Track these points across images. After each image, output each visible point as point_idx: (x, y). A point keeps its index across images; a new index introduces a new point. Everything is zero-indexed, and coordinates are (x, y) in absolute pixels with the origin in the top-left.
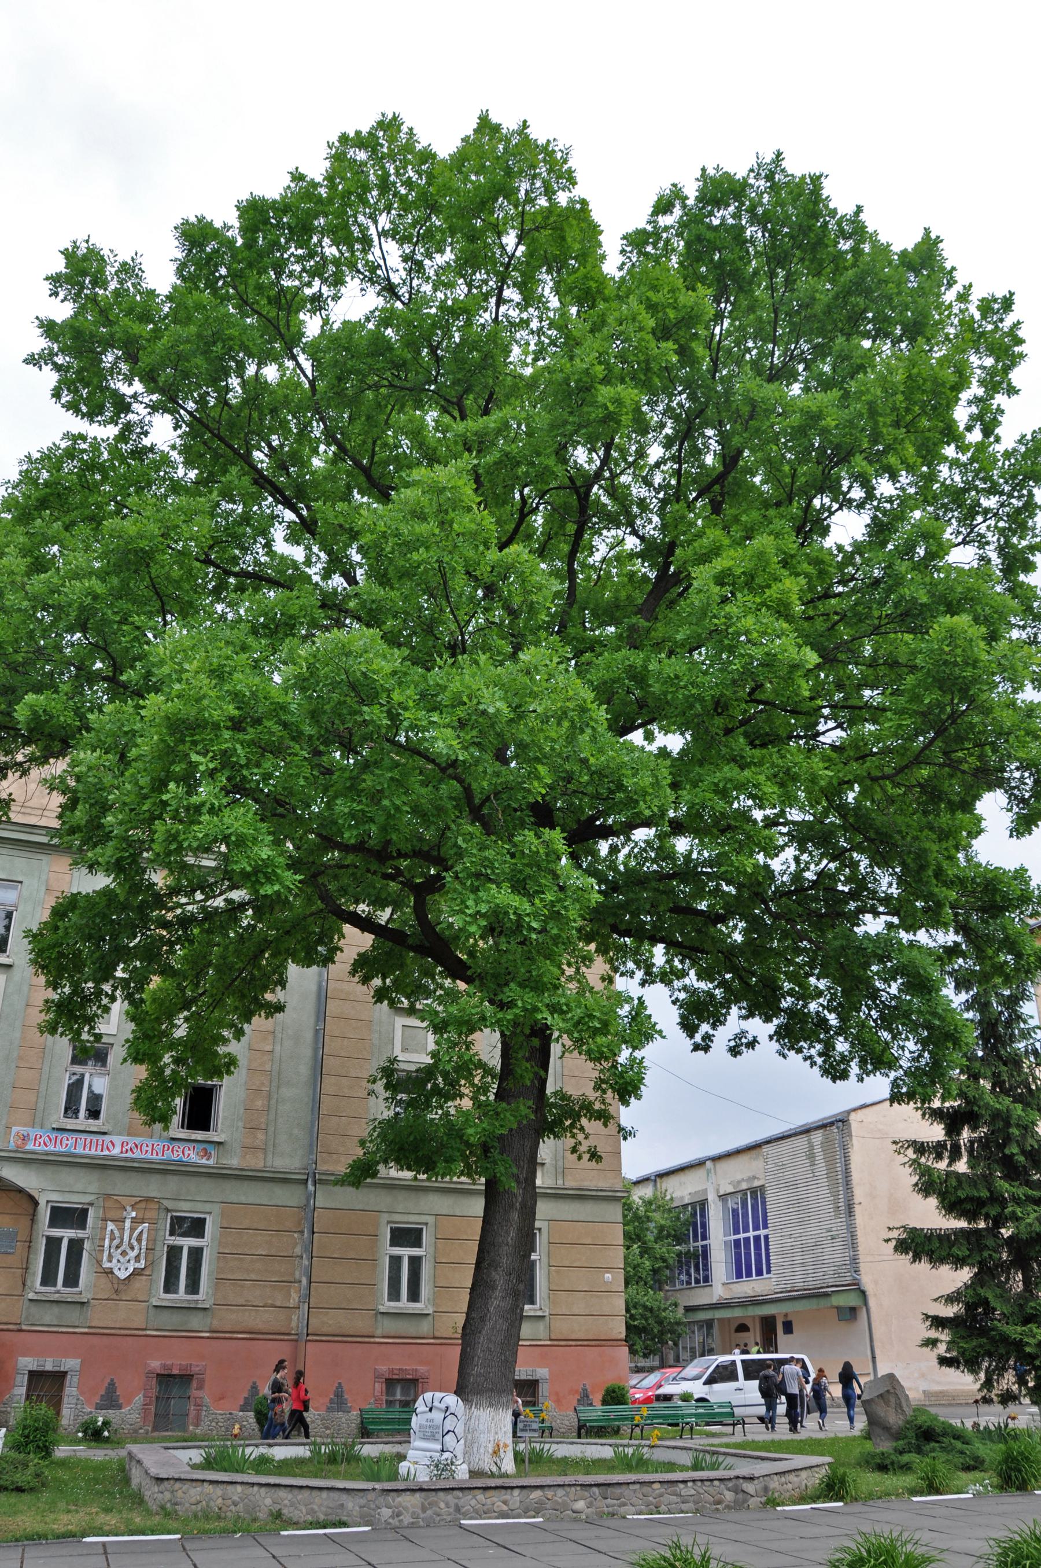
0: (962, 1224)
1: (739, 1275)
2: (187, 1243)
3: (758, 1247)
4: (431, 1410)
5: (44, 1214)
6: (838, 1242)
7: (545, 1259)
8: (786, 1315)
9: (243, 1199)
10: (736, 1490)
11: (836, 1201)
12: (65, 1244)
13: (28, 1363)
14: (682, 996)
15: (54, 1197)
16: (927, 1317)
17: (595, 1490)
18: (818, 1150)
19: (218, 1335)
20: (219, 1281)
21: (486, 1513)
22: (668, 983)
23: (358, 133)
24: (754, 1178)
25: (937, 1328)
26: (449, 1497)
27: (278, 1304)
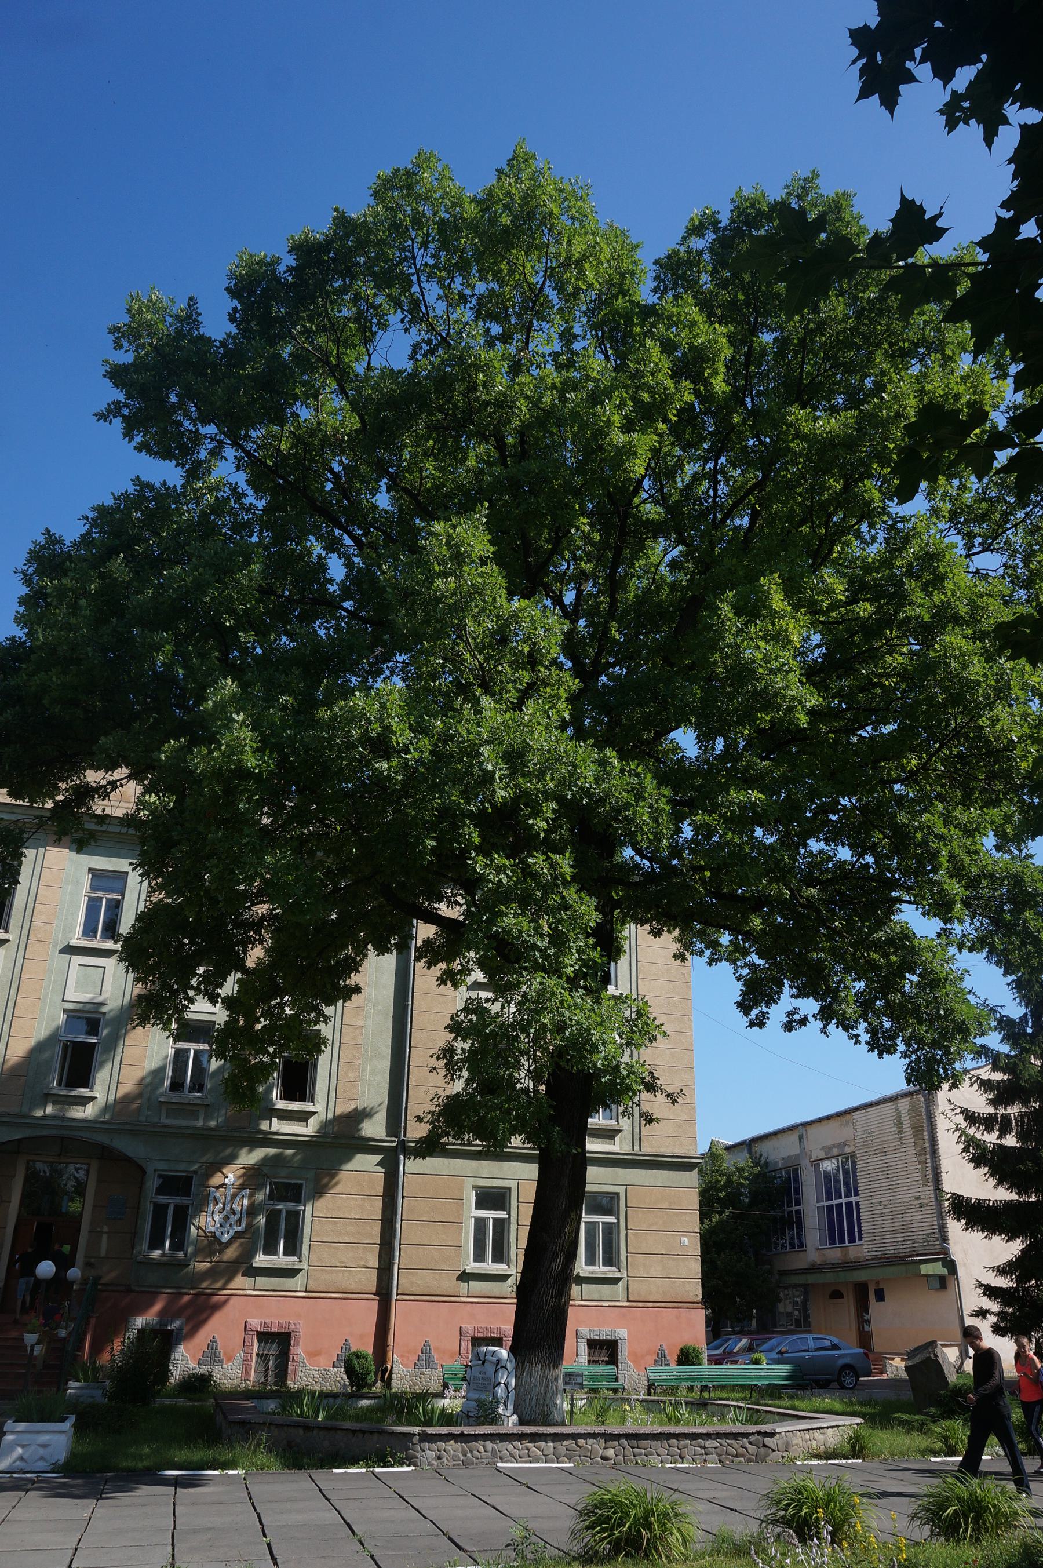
0: (1013, 1196)
1: (833, 1241)
4: (483, 1363)
5: (153, 1183)
6: (926, 1210)
11: (924, 1170)
12: (171, 1208)
14: (745, 972)
15: (162, 1166)
16: (981, 1285)
18: (905, 1117)
22: (733, 962)
23: (23, 601)
24: (845, 1144)
25: (989, 1297)
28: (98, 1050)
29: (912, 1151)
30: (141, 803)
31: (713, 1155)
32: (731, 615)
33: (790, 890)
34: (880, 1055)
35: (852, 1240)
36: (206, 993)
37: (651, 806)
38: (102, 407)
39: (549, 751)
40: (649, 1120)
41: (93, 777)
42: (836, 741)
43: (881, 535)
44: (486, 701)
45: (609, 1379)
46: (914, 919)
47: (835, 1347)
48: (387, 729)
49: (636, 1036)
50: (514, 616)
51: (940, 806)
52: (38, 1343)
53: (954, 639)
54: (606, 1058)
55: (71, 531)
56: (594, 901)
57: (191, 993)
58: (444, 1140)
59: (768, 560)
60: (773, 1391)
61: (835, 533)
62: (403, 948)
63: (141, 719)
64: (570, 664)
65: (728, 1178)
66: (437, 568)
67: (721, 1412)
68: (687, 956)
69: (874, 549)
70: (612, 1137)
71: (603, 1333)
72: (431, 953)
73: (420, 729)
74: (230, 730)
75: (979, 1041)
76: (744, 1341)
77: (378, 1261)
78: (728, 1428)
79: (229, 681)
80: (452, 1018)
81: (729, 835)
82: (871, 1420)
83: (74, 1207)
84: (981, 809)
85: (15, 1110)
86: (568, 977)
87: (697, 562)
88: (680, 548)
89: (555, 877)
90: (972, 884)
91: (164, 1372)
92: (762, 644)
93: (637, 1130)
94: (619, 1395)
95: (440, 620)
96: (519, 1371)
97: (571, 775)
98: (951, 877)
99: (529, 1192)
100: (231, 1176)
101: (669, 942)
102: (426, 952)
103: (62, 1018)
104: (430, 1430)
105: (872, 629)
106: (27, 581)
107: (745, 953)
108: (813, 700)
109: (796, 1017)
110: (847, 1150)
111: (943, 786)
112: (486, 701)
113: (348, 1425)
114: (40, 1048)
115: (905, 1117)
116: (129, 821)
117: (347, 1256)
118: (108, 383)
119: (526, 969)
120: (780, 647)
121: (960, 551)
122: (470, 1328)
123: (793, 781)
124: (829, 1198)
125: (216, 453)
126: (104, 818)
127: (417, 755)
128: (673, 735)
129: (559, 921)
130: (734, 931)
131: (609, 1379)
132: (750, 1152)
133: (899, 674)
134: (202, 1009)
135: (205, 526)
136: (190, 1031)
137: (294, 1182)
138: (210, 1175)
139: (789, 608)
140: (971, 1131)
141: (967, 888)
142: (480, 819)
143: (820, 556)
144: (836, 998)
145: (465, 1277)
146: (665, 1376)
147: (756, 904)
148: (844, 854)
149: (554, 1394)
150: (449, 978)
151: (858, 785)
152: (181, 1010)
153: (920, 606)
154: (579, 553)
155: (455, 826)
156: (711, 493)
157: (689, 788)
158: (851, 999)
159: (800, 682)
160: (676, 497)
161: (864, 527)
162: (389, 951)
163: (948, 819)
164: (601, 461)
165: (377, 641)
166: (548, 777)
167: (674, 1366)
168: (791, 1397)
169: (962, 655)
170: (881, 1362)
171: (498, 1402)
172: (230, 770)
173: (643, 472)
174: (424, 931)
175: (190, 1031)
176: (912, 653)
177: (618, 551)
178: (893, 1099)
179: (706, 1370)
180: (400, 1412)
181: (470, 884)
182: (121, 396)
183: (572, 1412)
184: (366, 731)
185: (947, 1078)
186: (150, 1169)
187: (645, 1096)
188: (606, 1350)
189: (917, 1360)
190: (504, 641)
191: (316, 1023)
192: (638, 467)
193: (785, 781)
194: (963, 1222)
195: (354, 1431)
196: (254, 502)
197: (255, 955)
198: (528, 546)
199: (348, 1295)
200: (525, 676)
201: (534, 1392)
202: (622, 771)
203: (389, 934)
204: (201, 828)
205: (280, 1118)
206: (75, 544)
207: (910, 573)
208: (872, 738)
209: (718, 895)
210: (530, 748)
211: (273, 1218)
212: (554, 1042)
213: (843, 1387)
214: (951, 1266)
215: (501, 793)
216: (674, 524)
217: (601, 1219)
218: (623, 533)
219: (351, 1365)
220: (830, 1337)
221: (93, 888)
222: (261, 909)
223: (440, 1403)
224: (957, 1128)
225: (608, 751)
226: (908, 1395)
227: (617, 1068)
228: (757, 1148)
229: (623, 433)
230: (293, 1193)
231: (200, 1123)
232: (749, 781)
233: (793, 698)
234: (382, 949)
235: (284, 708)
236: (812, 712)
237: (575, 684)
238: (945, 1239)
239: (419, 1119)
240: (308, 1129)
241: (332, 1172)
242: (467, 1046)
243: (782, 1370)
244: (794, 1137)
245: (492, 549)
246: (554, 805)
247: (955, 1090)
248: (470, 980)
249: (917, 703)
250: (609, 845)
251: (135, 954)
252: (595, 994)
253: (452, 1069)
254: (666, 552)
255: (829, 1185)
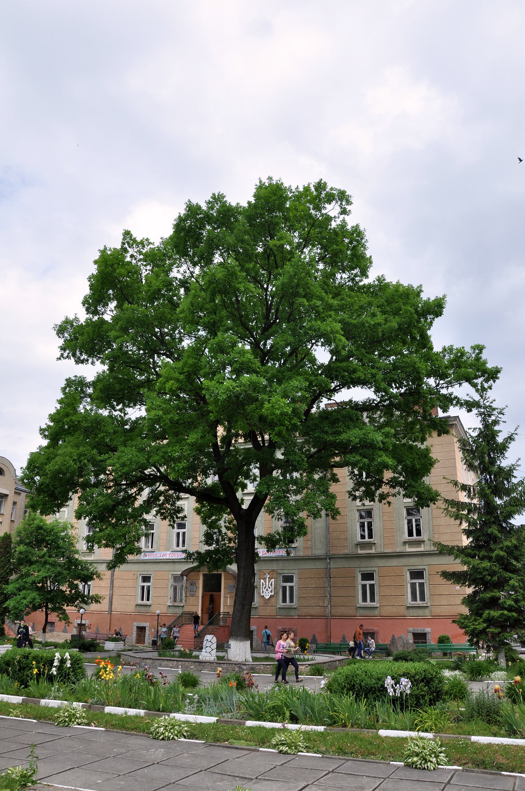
2: (288, 585)
7: (428, 582)
9: (305, 567)
10: (240, 668)
12: (417, 584)
13: (136, 624)
17: (197, 663)
19: (300, 617)
20: (299, 598)
21: (167, 667)
26: (158, 661)
27: (321, 605)
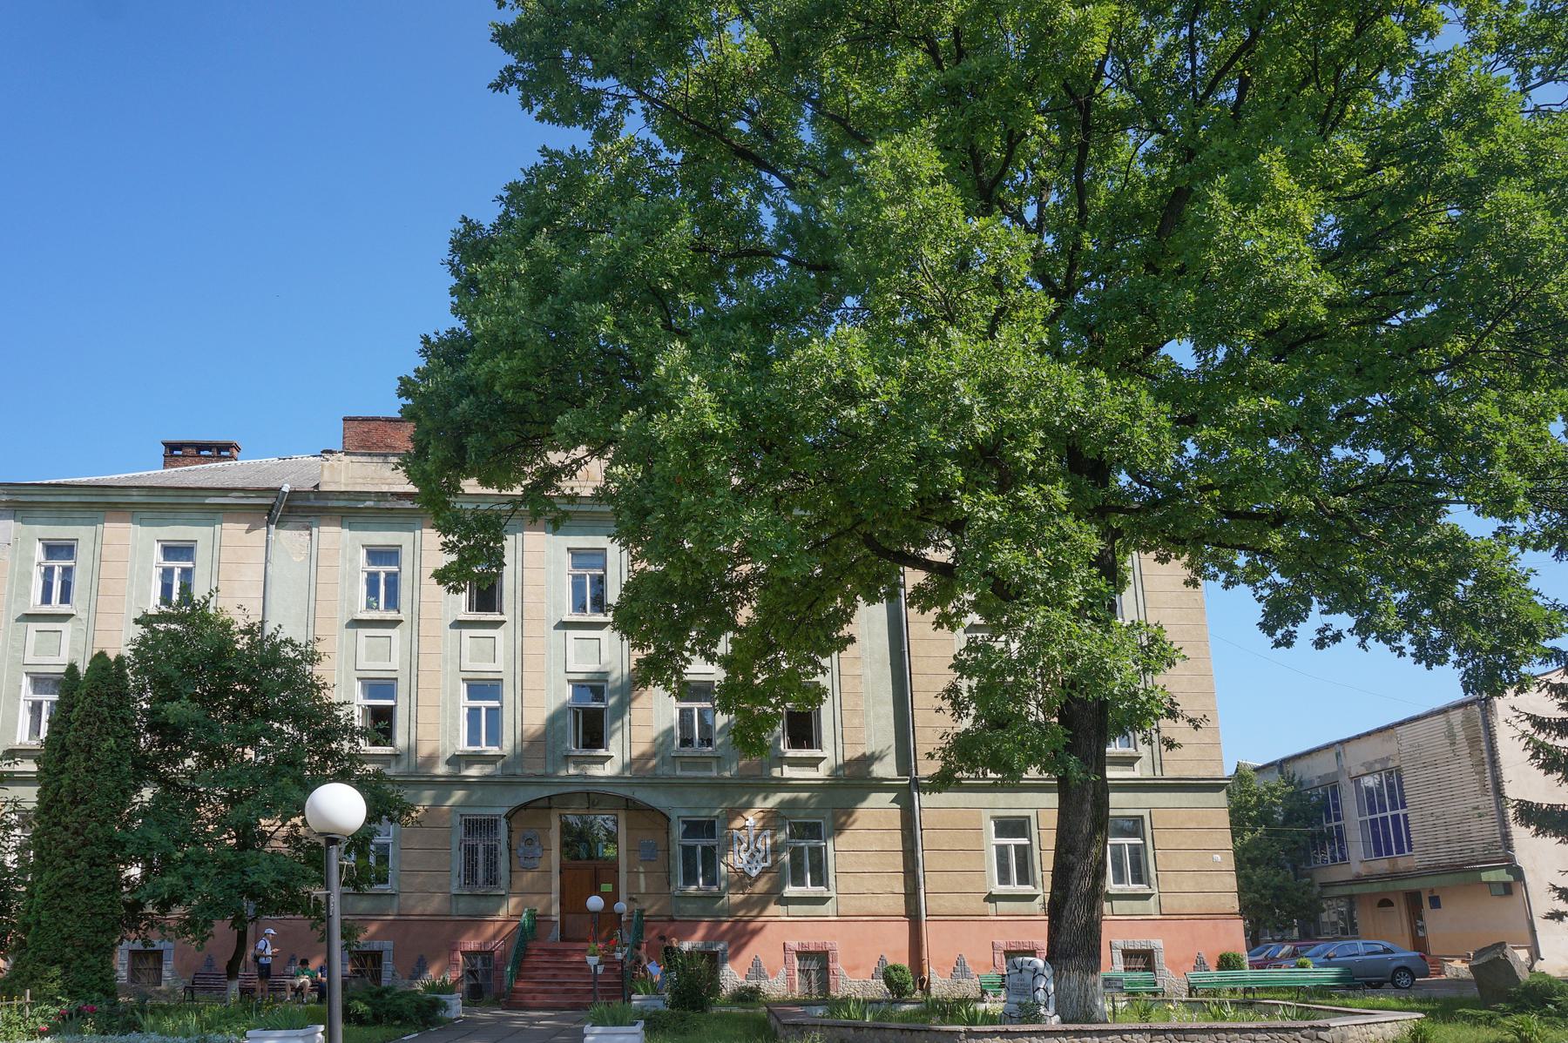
1: (1378, 853)
3: (1385, 826)
5: (678, 830)
8: (1432, 891)
14: (1266, 592)
15: (684, 813)
16: (1555, 888)
18: (1458, 729)
22: (1252, 583)
24: (1388, 759)
28: (607, 716)
29: (1468, 762)
30: (609, 477)
31: (1241, 776)
32: (1224, 204)
33: (1315, 501)
34: (1429, 667)
35: (1400, 850)
36: (703, 653)
37: (1149, 425)
38: (495, 77)
39: (1030, 377)
40: (1171, 745)
41: (555, 458)
42: (1360, 336)
43: (1406, 84)
44: (953, 333)
45: (1148, 983)
46: (1467, 521)
47: (1387, 951)
48: (851, 373)
49: (1153, 662)
50: (976, 237)
51: (1493, 394)
52: (600, 963)
53: (1510, 194)
54: (1122, 685)
55: (488, 215)
56: (1095, 529)
57: (687, 654)
58: (958, 775)
59: (1267, 130)
60: (1322, 992)
61: (1347, 90)
62: (892, 596)
63: (601, 391)
64: (1040, 286)
65: (1259, 797)
66: (883, 195)
67: (1270, 1010)
68: (1200, 580)
69: (1395, 105)
70: (1132, 764)
71: (1138, 944)
72: (922, 598)
73: (886, 371)
74: (685, 392)
75: (1549, 644)
76: (1287, 948)
77: (915, 884)
78: (1278, 1023)
79: (678, 344)
80: (955, 657)
81: (1238, 451)
82: (1432, 1015)
83: (610, 852)
84: (1547, 390)
85: (542, 771)
86: (1073, 609)
87: (1178, 149)
88: (1156, 137)
89: (1051, 508)
90: (1539, 474)
91: (715, 987)
92: (1265, 232)
93: (1157, 756)
94: (1160, 997)
95: (899, 250)
96: (1057, 978)
97: (1057, 400)
98: (1511, 469)
99: (1051, 819)
100: (751, 819)
101: (1177, 569)
102: (919, 597)
103: (568, 691)
104: (975, 1028)
105: (1396, 199)
106: (456, 272)
107: (1265, 573)
108: (1331, 289)
109: (1328, 633)
110: (1391, 764)
111: (1496, 370)
112: (953, 333)
113: (894, 1025)
114: (553, 720)
115: (1458, 729)
116: (601, 496)
117: (870, 883)
118: (496, 49)
119: (1027, 604)
120: (1283, 233)
121: (1513, 87)
122: (1002, 943)
123: (1312, 382)
124: (1373, 811)
125: (623, 105)
126: (573, 498)
127: (886, 398)
128: (1163, 351)
129: (1059, 552)
130: (1252, 550)
131: (1148, 983)
132: (1281, 772)
133: (1438, 246)
134: (699, 669)
135: (622, 188)
136: (688, 691)
137: (809, 829)
138: (730, 820)
139: (1296, 187)
140: (1541, 737)
141: (1531, 480)
142: (961, 457)
143: (1328, 121)
144: (1374, 610)
145: (991, 898)
146: (1205, 980)
147: (1279, 519)
148: (1376, 457)
149: (1093, 1001)
150: (944, 621)
151: (1391, 379)
152: (678, 672)
153: (1462, 160)
154: (1035, 161)
155: (935, 467)
156: (1188, 65)
157: (1191, 404)
158: (1392, 611)
159: (1314, 269)
160: (1145, 77)
161: (1384, 77)
162: (879, 600)
163: (1504, 406)
164: (1054, 45)
165: (823, 285)
166: (1032, 405)
167: (1214, 971)
168: (1343, 997)
169: (1520, 212)
170: (1439, 962)
171: (1039, 1004)
172: (692, 434)
173: (1104, 51)
174: (913, 578)
175: (688, 691)
176: (1450, 221)
177: (1083, 149)
178: (1444, 711)
179: (1248, 973)
180: (943, 1014)
181: (957, 526)
182: (511, 60)
183: (1114, 1013)
184: (829, 379)
185: (1512, 683)
186: (673, 816)
187: (1164, 723)
188: (1142, 959)
189: (1483, 960)
190: (964, 265)
191: (815, 674)
192: (1097, 46)
193: (1306, 383)
194: (1533, 828)
195: (902, 1030)
196: (670, 156)
197: (745, 614)
198: (976, 158)
199: (877, 917)
200: (994, 302)
201: (1075, 995)
202: (1113, 391)
203: (879, 586)
204: (673, 494)
205: (790, 765)
206: (495, 227)
207: (1447, 123)
208: (1405, 324)
209: (1231, 514)
210: (1009, 377)
211: (796, 854)
212: (1063, 672)
213: (1398, 987)
214: (1518, 873)
215: (981, 429)
216: (1147, 112)
217: (1126, 841)
218: (1087, 127)
219: (889, 976)
220: (1383, 939)
221: (575, 566)
222: (745, 569)
223: (981, 1007)
224: (1524, 735)
225: (1095, 372)
226: (1474, 992)
227: (1134, 695)
228: (1289, 768)
229: (1075, 8)
230: (812, 830)
231: (714, 774)
232: (1260, 387)
233: (1307, 288)
234: (872, 599)
235: (738, 366)
236: (1330, 304)
237: (1051, 305)
238: (1509, 847)
239: (931, 756)
240: (822, 772)
241: (849, 811)
242: (974, 682)
243: (1331, 973)
244: (1331, 755)
245: (942, 166)
246: (1042, 434)
247: (1521, 696)
248: (967, 621)
249: (1463, 276)
250: (1100, 471)
251: (628, 622)
252: (1105, 624)
253: (958, 708)
254: (1137, 145)
255: (1372, 800)
